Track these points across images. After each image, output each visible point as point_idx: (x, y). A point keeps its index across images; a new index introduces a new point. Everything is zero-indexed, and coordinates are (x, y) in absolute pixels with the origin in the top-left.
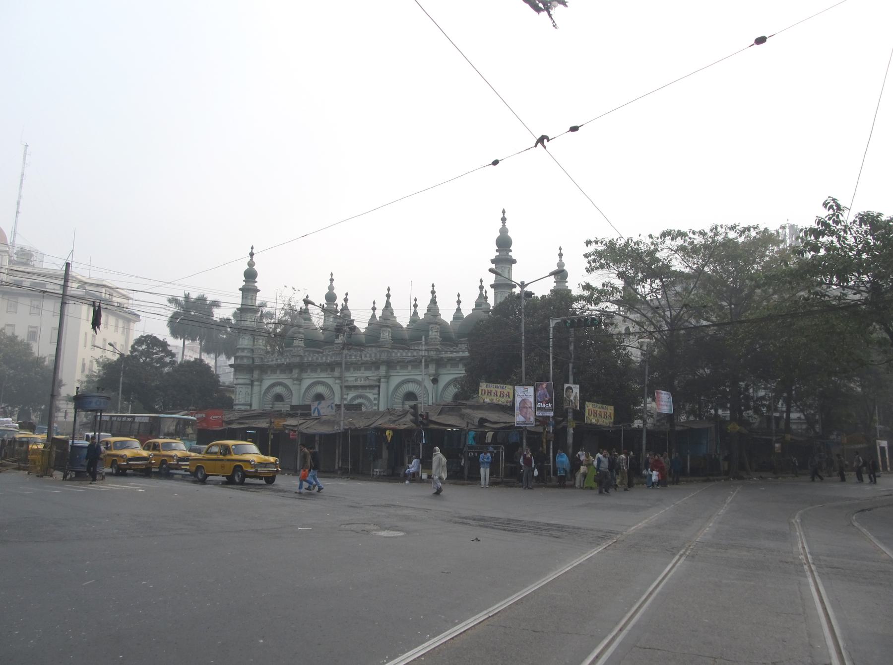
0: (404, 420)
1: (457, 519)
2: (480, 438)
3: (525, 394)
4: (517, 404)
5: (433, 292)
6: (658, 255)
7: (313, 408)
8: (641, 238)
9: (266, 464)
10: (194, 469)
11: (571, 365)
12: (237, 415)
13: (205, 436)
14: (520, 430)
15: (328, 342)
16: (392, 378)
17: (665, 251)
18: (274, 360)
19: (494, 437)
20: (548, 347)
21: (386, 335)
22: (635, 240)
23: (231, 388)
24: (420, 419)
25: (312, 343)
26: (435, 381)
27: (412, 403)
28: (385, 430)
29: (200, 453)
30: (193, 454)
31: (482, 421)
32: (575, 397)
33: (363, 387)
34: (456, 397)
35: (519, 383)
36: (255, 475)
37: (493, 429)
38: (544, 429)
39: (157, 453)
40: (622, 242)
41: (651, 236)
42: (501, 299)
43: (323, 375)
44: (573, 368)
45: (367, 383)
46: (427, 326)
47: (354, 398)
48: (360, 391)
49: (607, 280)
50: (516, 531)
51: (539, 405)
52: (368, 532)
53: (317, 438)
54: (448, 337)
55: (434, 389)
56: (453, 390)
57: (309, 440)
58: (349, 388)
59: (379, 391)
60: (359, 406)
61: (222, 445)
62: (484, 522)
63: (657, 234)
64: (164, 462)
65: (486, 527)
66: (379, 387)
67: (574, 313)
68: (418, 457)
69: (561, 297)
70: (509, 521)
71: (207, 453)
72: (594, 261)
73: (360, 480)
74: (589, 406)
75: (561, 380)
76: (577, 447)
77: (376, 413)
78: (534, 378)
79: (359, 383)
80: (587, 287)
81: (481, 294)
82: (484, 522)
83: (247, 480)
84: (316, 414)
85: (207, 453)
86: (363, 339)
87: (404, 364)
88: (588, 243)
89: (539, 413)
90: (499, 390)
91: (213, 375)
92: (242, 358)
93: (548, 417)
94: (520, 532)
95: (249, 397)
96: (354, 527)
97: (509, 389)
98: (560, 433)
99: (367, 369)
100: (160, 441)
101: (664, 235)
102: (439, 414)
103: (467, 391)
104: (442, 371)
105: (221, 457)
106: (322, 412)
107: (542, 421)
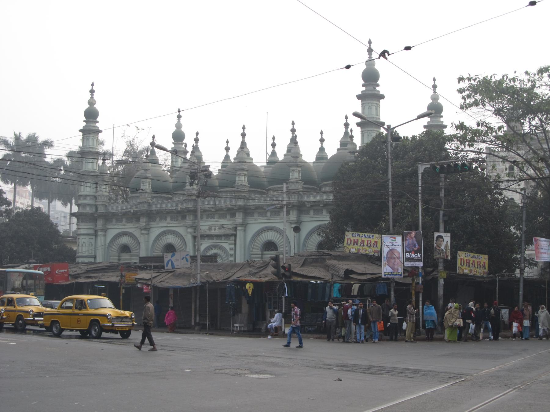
0: (265, 272)
1: (322, 366)
2: (346, 291)
3: (392, 244)
4: (384, 255)
5: (293, 131)
6: (536, 90)
7: (166, 261)
8: (517, 74)
9: (122, 319)
10: (48, 324)
11: (441, 213)
12: (84, 268)
13: (52, 292)
14: (387, 281)
15: (179, 187)
16: (249, 226)
17: (544, 87)
18: (119, 207)
19: (361, 289)
20: (417, 194)
21: (242, 180)
22: (511, 76)
23: (74, 238)
24: (282, 271)
25: (161, 190)
26: (297, 229)
27: (272, 254)
28: (244, 283)
29: (52, 308)
30: (48, 309)
31: (348, 272)
32: (446, 246)
33: (219, 236)
34: (320, 246)
35: (387, 232)
36: (112, 330)
37: (359, 281)
38: (413, 280)
39: (12, 308)
40: (498, 78)
41: (527, 73)
42: (368, 140)
43: (174, 223)
44: (444, 215)
45: (222, 232)
46: (285, 170)
47: (208, 249)
48: (215, 241)
49: (483, 119)
50: (376, 374)
51: (408, 255)
52: (240, 375)
53: (171, 292)
54: (311, 180)
55: (295, 238)
56: (317, 239)
57: (162, 294)
58: (203, 237)
59: (235, 241)
60: (214, 258)
61: (77, 300)
62: (345, 367)
63: (534, 70)
64: (20, 317)
65: (349, 371)
66: (235, 236)
67: (447, 156)
68: (280, 311)
69: (434, 137)
70: (370, 367)
71: (61, 307)
72: (469, 96)
73: (221, 335)
74: (461, 255)
75: (430, 228)
76: (447, 299)
77: (234, 265)
78: (401, 227)
79: (213, 232)
80: (461, 126)
81: (346, 133)
82: (345, 367)
83: (104, 334)
84: (170, 266)
85: (61, 307)
86: (216, 183)
87: (261, 210)
88: (461, 79)
89: (408, 264)
90: (366, 239)
91: (52, 224)
92: (84, 206)
93: (418, 267)
94: (379, 374)
95: (93, 249)
96: (228, 371)
97: (376, 237)
98: (430, 285)
99: (222, 216)
100: (15, 296)
101: (541, 71)
102: (303, 265)
103: (332, 239)
104: (305, 218)
105: (77, 311)
106: (176, 264)
107: (411, 272)
